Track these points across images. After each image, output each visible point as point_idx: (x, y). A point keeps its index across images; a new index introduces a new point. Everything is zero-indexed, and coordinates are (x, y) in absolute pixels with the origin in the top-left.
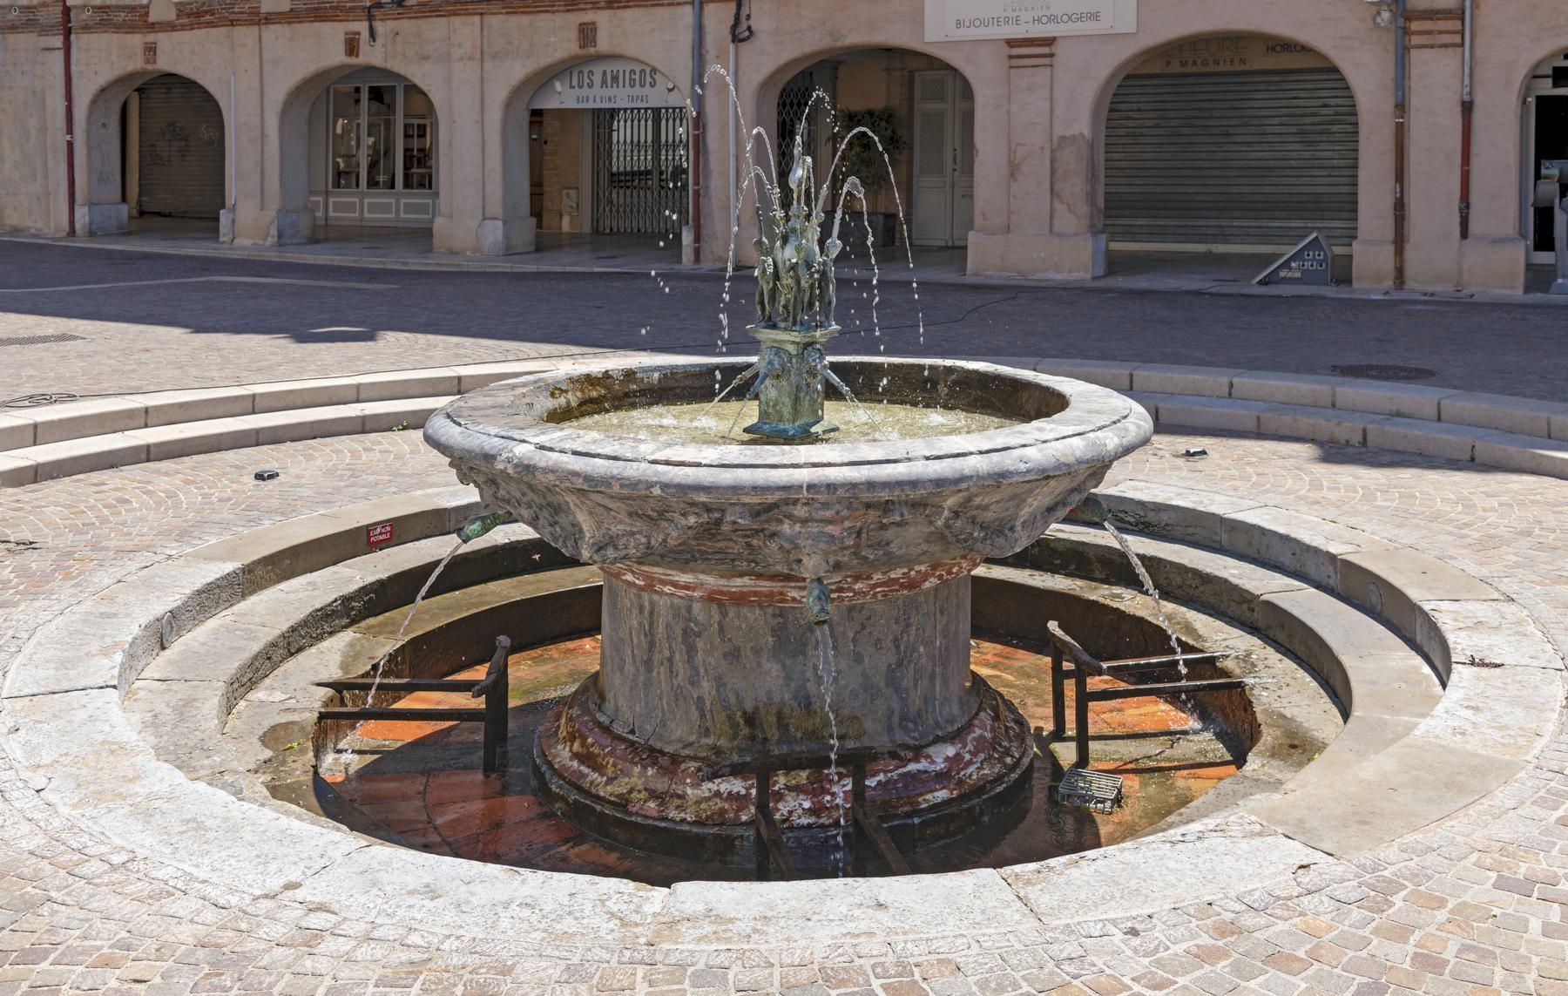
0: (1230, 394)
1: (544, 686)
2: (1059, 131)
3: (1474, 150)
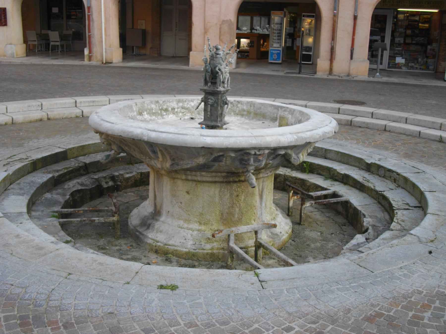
0: (76, 106)
1: (323, 261)
2: (223, 18)
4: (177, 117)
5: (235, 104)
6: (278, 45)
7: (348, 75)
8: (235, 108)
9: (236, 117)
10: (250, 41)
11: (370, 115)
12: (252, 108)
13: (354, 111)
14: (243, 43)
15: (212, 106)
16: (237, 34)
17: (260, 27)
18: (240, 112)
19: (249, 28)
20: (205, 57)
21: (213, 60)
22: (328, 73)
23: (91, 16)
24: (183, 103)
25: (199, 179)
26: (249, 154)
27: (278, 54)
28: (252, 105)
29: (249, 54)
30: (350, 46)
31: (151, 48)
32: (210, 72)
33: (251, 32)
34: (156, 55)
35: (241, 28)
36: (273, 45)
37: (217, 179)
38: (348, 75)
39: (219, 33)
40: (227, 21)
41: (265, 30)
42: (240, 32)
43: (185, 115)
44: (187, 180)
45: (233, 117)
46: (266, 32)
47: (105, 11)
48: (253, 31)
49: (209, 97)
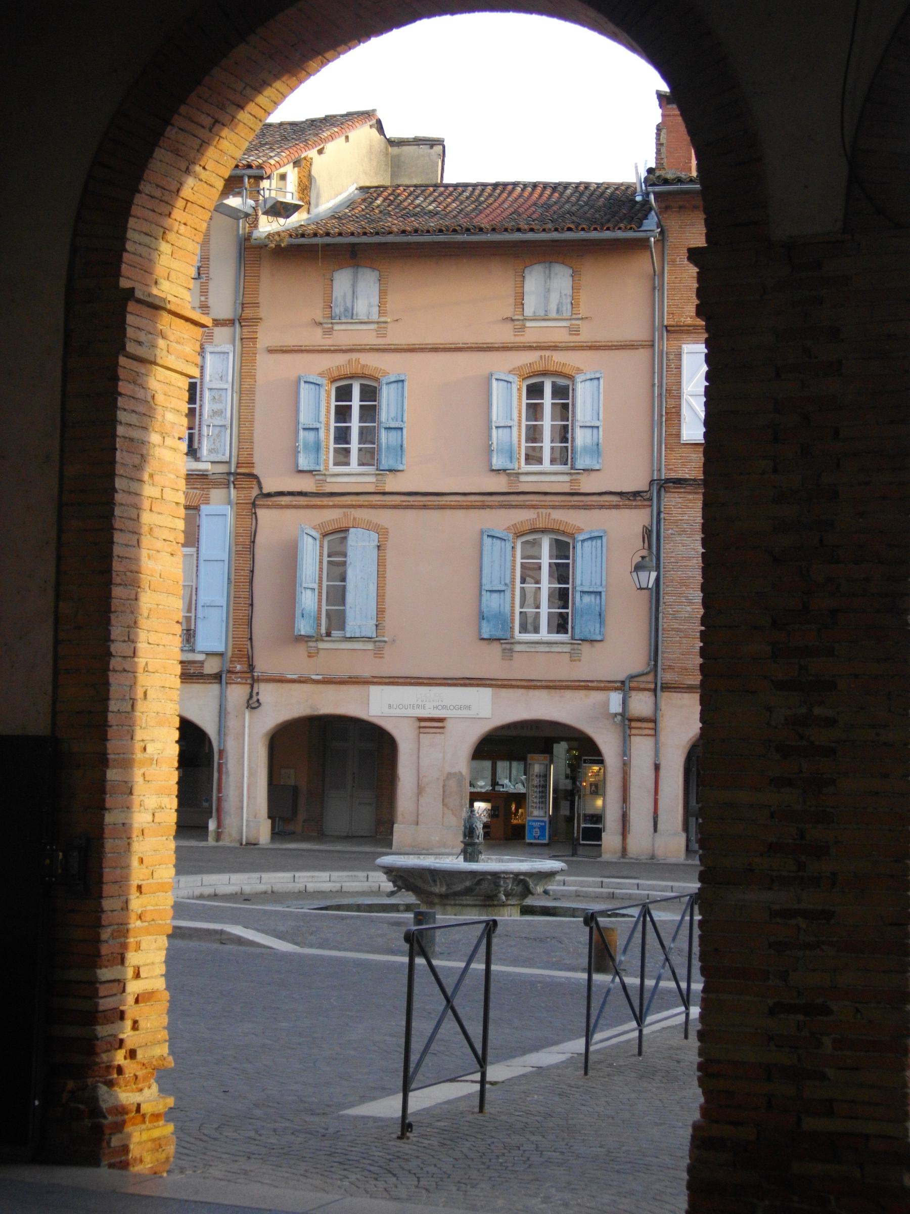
3: (660, 788)
6: (542, 813)
7: (653, 857)
10: (492, 807)
11: (636, 887)
13: (618, 883)
15: (470, 854)
17: (510, 781)
22: (620, 855)
23: (224, 766)
25: (465, 902)
26: (500, 877)
27: (542, 828)
30: (652, 810)
31: (304, 821)
33: (493, 789)
34: (316, 834)
36: (532, 813)
37: (477, 903)
38: (653, 857)
39: (442, 793)
40: (455, 774)
41: (520, 786)
42: (473, 790)
44: (455, 905)
46: (520, 789)
47: (249, 756)
48: (497, 788)
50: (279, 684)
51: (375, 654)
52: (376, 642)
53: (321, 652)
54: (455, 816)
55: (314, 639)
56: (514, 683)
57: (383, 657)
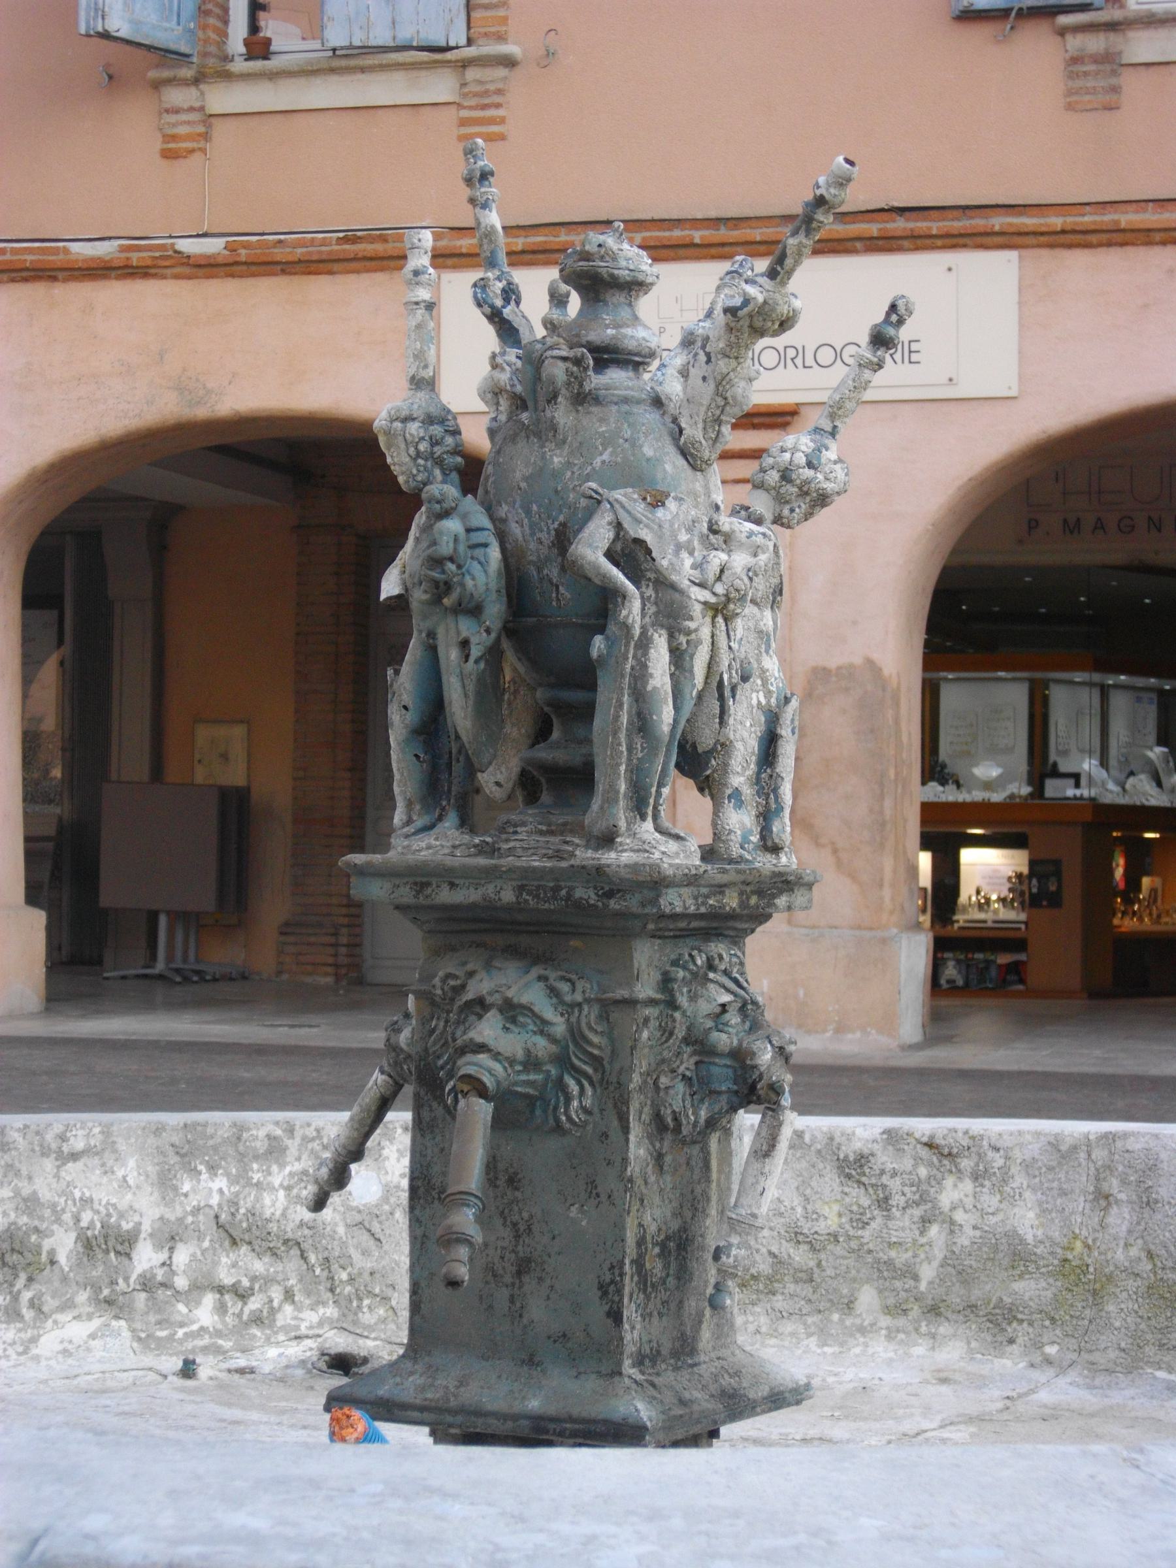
4: (146, 1342)
5: (895, 1184)
8: (903, 1225)
9: (920, 1350)
10: (1032, 863)
12: (1120, 1219)
14: (978, 882)
16: (929, 811)
17: (1104, 763)
18: (965, 1277)
19: (1023, 767)
20: (419, 402)
21: (544, 432)
24: (241, 1178)
28: (1113, 1185)
29: (1023, 957)
31: (286, 929)
32: (495, 611)
33: (1039, 792)
35: (955, 766)
40: (847, 673)
42: (948, 794)
43: (257, 1320)
45: (881, 1348)
48: (1052, 788)
49: (481, 986)
50: (37, 291)
51: (463, 122)
52: (465, 64)
53: (220, 129)
54: (853, 876)
55: (187, 73)
56: (1127, 218)
57: (502, 137)
